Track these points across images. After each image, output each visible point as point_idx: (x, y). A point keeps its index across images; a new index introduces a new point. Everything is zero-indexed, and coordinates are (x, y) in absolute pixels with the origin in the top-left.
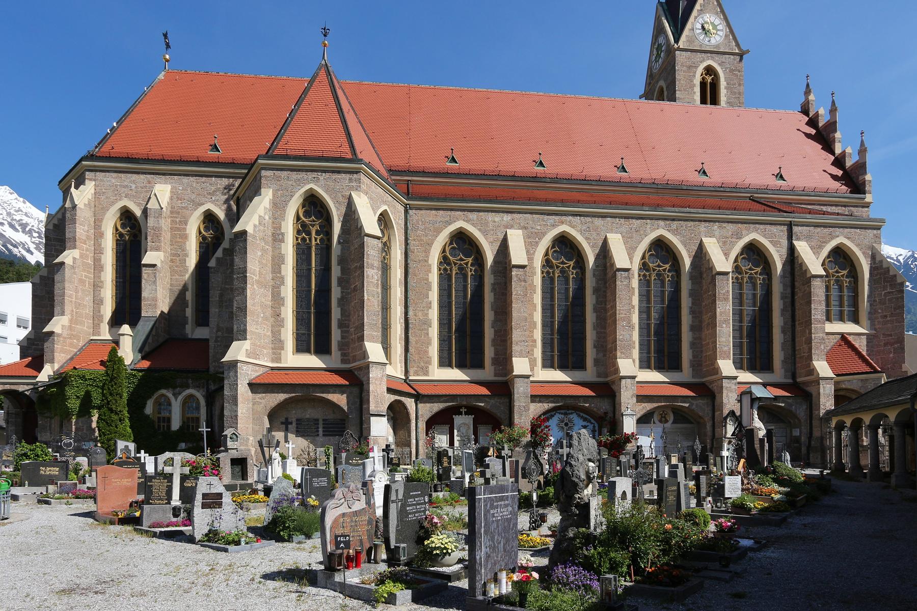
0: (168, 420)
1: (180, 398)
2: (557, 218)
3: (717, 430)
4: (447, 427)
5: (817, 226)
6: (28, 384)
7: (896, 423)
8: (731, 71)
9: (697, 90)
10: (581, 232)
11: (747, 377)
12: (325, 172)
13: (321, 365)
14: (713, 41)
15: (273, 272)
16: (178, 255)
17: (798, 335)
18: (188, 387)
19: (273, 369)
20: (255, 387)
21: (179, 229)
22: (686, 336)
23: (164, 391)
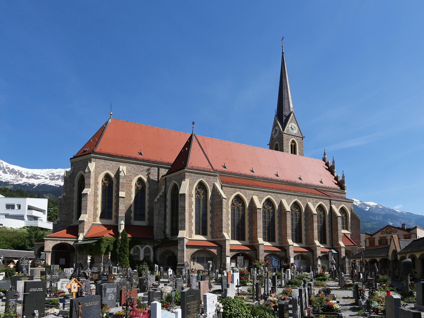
0: (138, 256)
1: (144, 248)
2: (267, 193)
3: (314, 262)
4: (235, 260)
5: (337, 201)
6: (72, 241)
7: (419, 258)
8: (300, 142)
9: (290, 147)
10: (274, 198)
11: (296, 245)
12: (206, 175)
13: (205, 239)
14: (294, 132)
15: (189, 207)
16: (129, 193)
17: (333, 233)
18: (146, 244)
19: (189, 240)
20: (188, 246)
21: (128, 183)
22: (303, 232)
23: (137, 246)
